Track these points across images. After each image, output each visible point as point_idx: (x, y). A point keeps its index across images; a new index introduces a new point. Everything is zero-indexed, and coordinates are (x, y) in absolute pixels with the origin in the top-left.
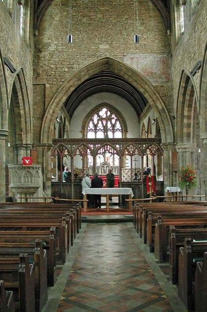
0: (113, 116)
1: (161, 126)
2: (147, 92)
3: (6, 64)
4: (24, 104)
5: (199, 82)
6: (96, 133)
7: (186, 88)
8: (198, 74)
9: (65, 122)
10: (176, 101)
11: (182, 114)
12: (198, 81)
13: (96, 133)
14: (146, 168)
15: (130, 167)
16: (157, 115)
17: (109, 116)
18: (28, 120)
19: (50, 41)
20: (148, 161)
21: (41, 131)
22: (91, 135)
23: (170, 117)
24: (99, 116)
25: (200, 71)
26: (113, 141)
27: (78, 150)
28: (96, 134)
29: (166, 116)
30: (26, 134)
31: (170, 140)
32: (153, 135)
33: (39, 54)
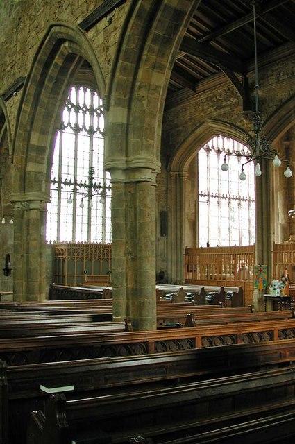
5: (16, 113)
12: (15, 110)
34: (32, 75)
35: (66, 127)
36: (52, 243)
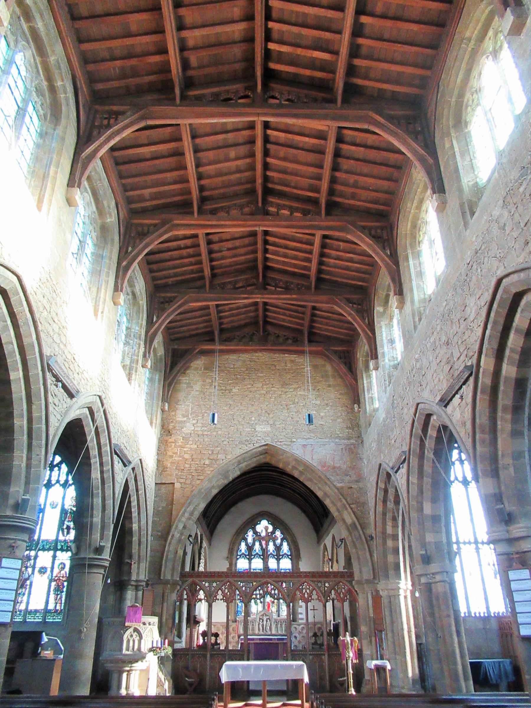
0: (278, 533)
1: (352, 551)
2: (328, 497)
3: (116, 453)
4: (139, 514)
5: (405, 484)
6: (250, 560)
7: (386, 491)
8: (403, 470)
9: (201, 542)
10: (373, 510)
11: (384, 532)
13: (250, 560)
14: (332, 622)
15: (304, 621)
16: (344, 534)
17: (271, 533)
18: (144, 540)
19: (185, 419)
20: (335, 610)
21: (162, 560)
22: (242, 564)
23: (365, 537)
24: (255, 532)
25: (405, 465)
26: (277, 577)
27: (220, 592)
28: (250, 563)
29: (360, 535)
30: (139, 564)
31: (367, 574)
32: (339, 567)
33: (166, 438)
34: (412, 449)
35: (453, 482)
36: (482, 615)
